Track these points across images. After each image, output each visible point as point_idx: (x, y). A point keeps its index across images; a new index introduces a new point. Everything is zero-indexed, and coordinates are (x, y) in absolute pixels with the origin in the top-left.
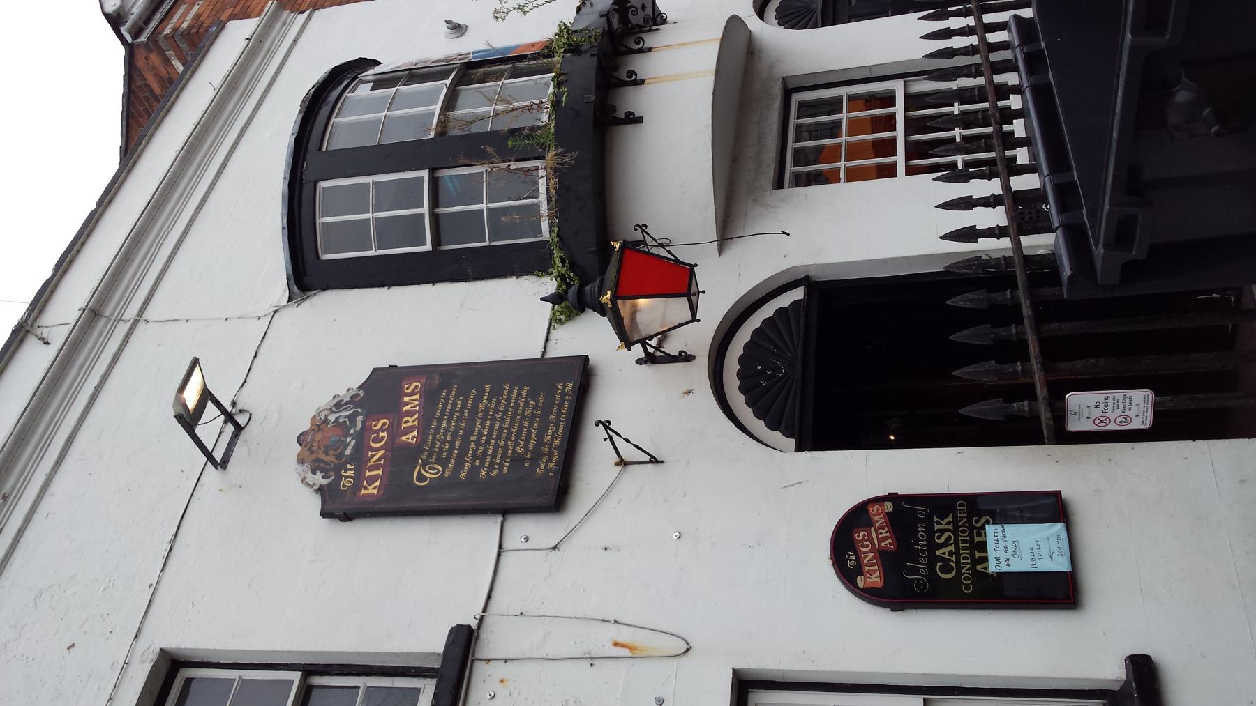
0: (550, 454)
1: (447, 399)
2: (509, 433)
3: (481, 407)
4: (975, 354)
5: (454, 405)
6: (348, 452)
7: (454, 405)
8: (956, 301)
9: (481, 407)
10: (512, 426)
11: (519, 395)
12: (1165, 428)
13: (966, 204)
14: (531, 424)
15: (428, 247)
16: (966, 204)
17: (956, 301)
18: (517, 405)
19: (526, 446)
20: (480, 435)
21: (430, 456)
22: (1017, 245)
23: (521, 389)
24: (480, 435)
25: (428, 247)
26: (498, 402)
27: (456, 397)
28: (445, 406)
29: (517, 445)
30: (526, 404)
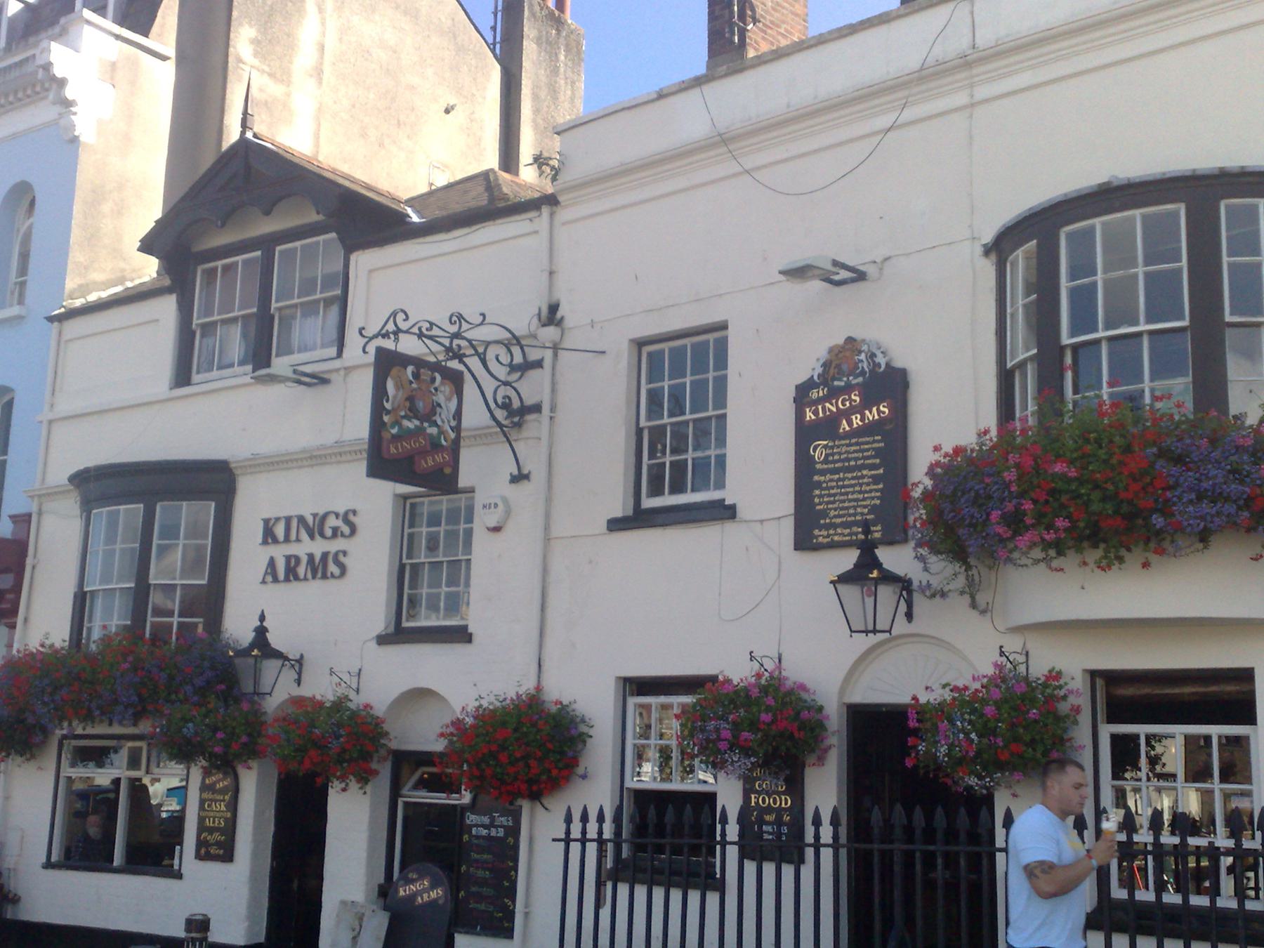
0: (828, 536)
1: (874, 441)
2: (844, 501)
3: (865, 472)
4: (929, 818)
5: (868, 450)
6: (836, 383)
7: (868, 450)
8: (939, 811)
9: (865, 472)
10: (850, 501)
11: (873, 498)
12: (181, 844)
13: (601, 818)
14: (850, 515)
15: (1228, 318)
16: (601, 818)
17: (939, 811)
18: (864, 499)
19: (835, 517)
20: (843, 480)
21: (832, 448)
22: (625, 841)
23: (878, 498)
24: (843, 480)
25: (1228, 318)
26: (868, 484)
27: (873, 449)
28: (867, 443)
29: (835, 509)
30: (865, 507)
